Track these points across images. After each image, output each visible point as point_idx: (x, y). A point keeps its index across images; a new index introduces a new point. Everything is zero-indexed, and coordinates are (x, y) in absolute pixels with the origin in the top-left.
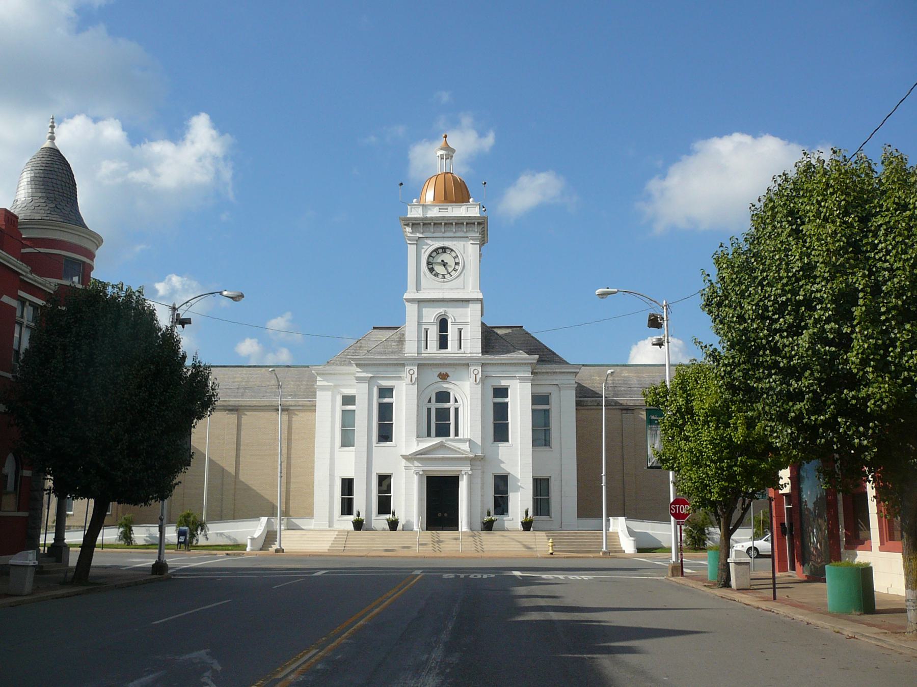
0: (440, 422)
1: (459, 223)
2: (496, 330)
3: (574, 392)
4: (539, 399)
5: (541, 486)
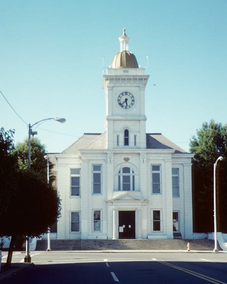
2: (151, 136)
3: (191, 167)
4: (175, 171)
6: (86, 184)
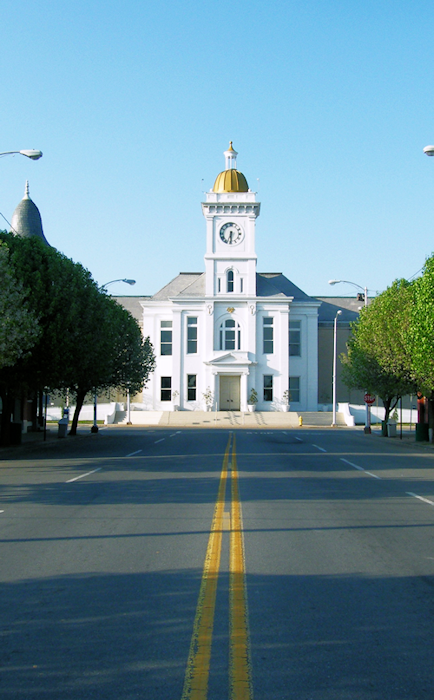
0: (228, 339)
1: (241, 207)
5: (294, 382)
6: (178, 341)
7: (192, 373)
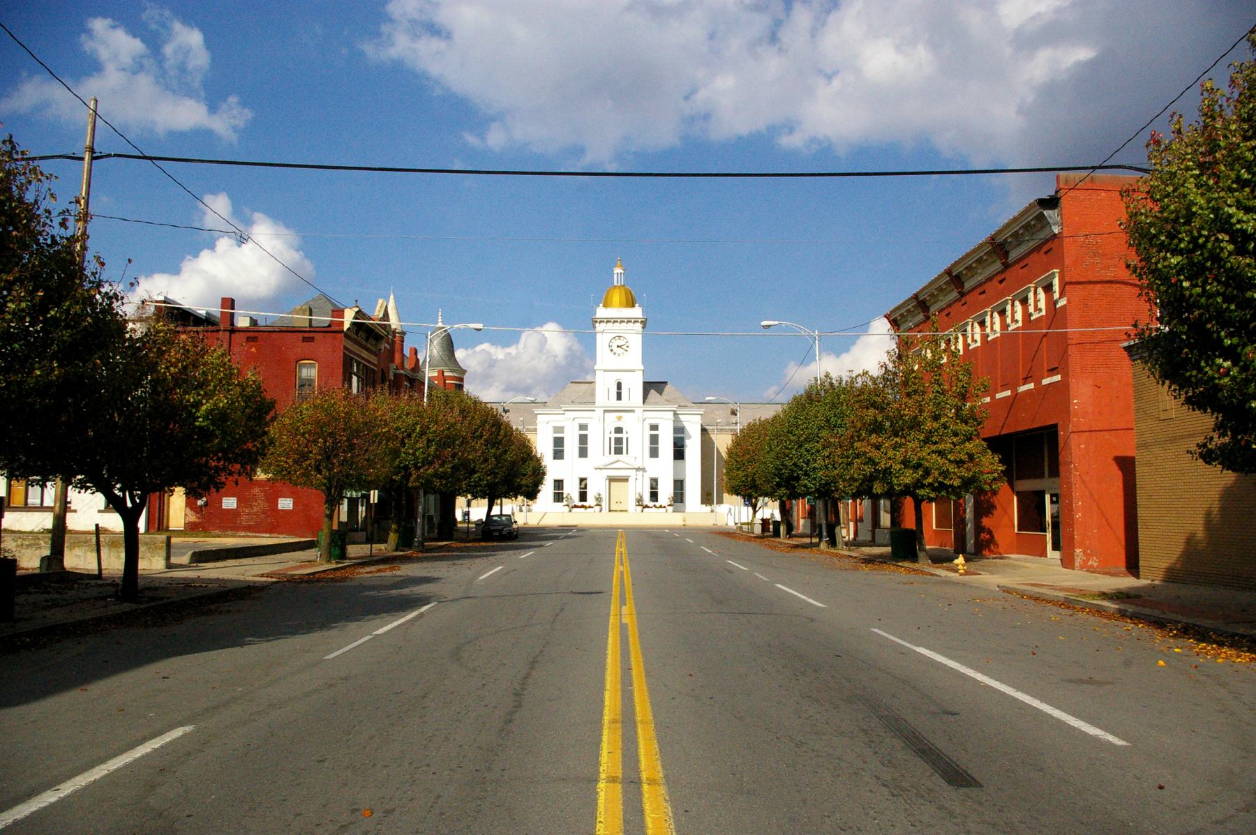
7: (654, 476)
